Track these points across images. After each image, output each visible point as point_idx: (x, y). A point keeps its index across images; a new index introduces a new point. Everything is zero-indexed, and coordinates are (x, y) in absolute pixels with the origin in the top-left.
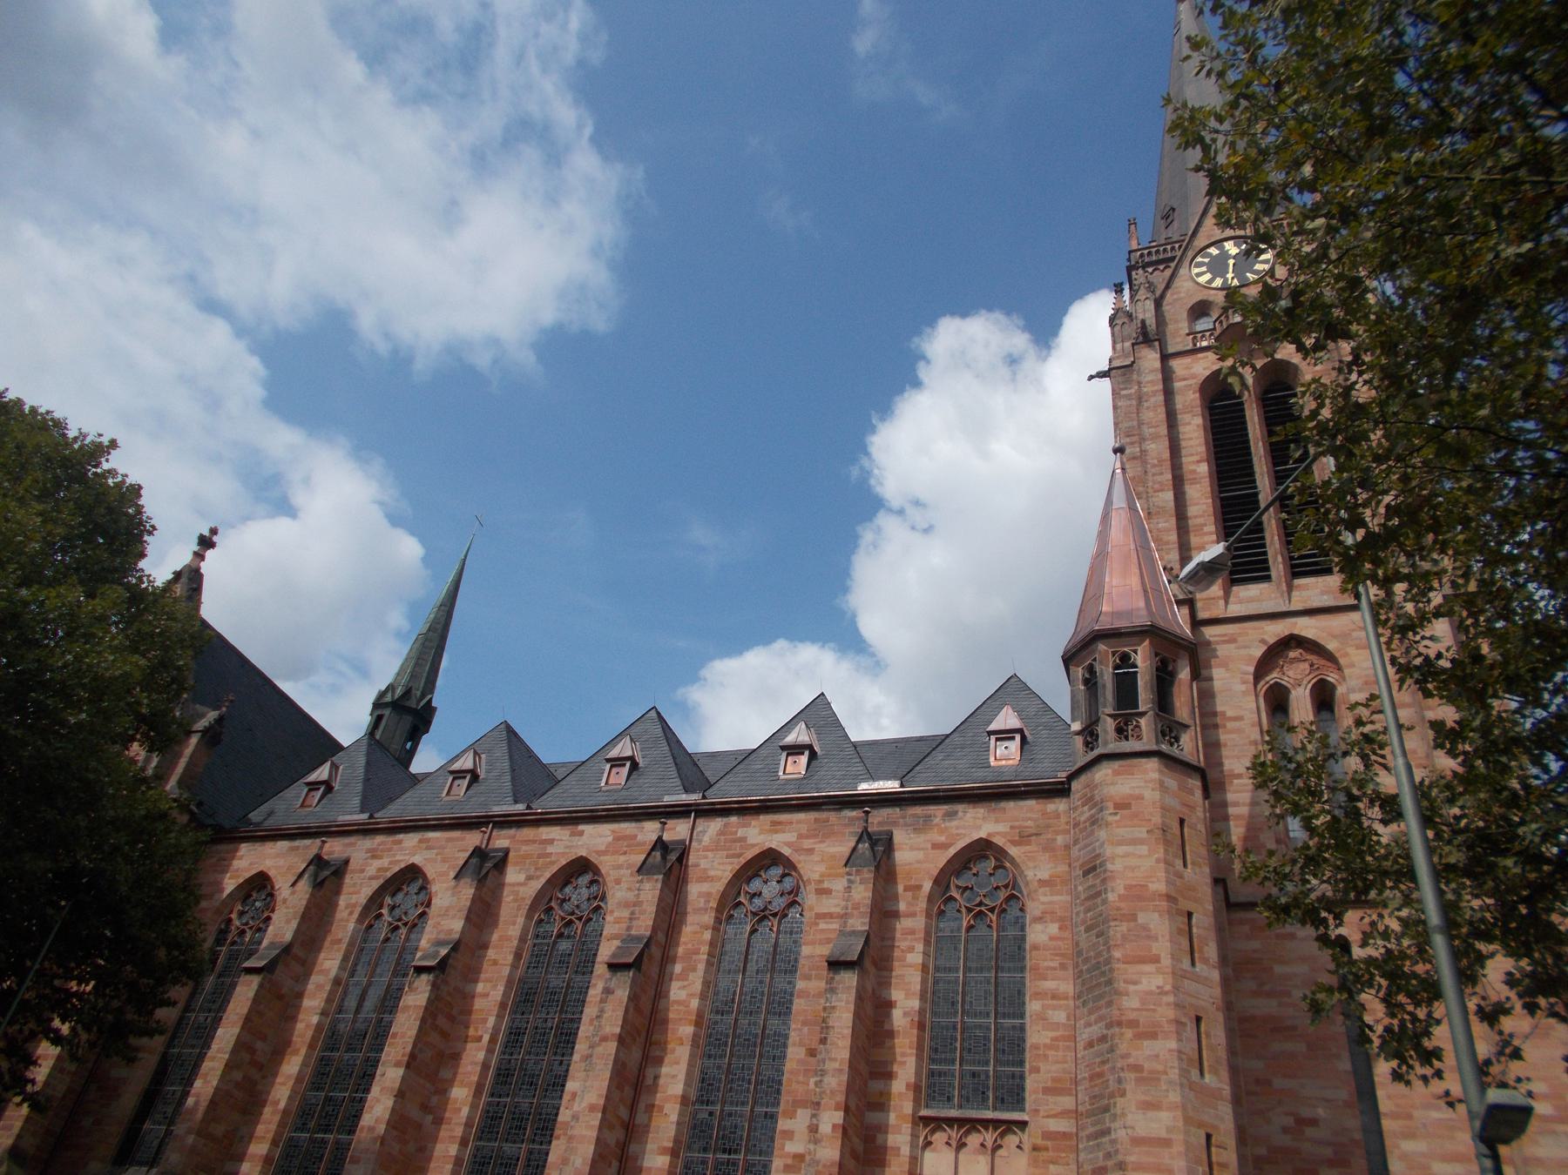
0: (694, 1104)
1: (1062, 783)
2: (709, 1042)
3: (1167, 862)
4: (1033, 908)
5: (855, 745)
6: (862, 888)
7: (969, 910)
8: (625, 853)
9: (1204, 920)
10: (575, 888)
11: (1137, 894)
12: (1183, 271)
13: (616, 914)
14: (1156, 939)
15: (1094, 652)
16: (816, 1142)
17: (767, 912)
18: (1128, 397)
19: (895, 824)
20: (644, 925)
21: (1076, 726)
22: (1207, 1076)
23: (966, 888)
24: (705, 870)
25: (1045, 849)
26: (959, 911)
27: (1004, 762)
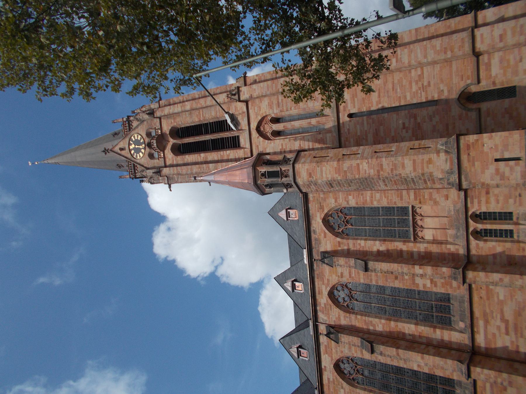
0: (417, 321)
1: (303, 195)
2: (395, 316)
3: (328, 161)
4: (344, 204)
5: (292, 266)
6: (340, 261)
7: (346, 225)
8: (332, 349)
9: (344, 151)
10: (345, 369)
11: (338, 170)
12: (138, 161)
13: (353, 352)
14: (352, 165)
15: (261, 185)
16: (426, 275)
17: (350, 295)
18: (178, 178)
19: (318, 251)
20: (356, 340)
21: (285, 191)
22: (393, 150)
23: (339, 226)
24: (336, 318)
25: (325, 201)
26: (346, 229)
27: (297, 215)
